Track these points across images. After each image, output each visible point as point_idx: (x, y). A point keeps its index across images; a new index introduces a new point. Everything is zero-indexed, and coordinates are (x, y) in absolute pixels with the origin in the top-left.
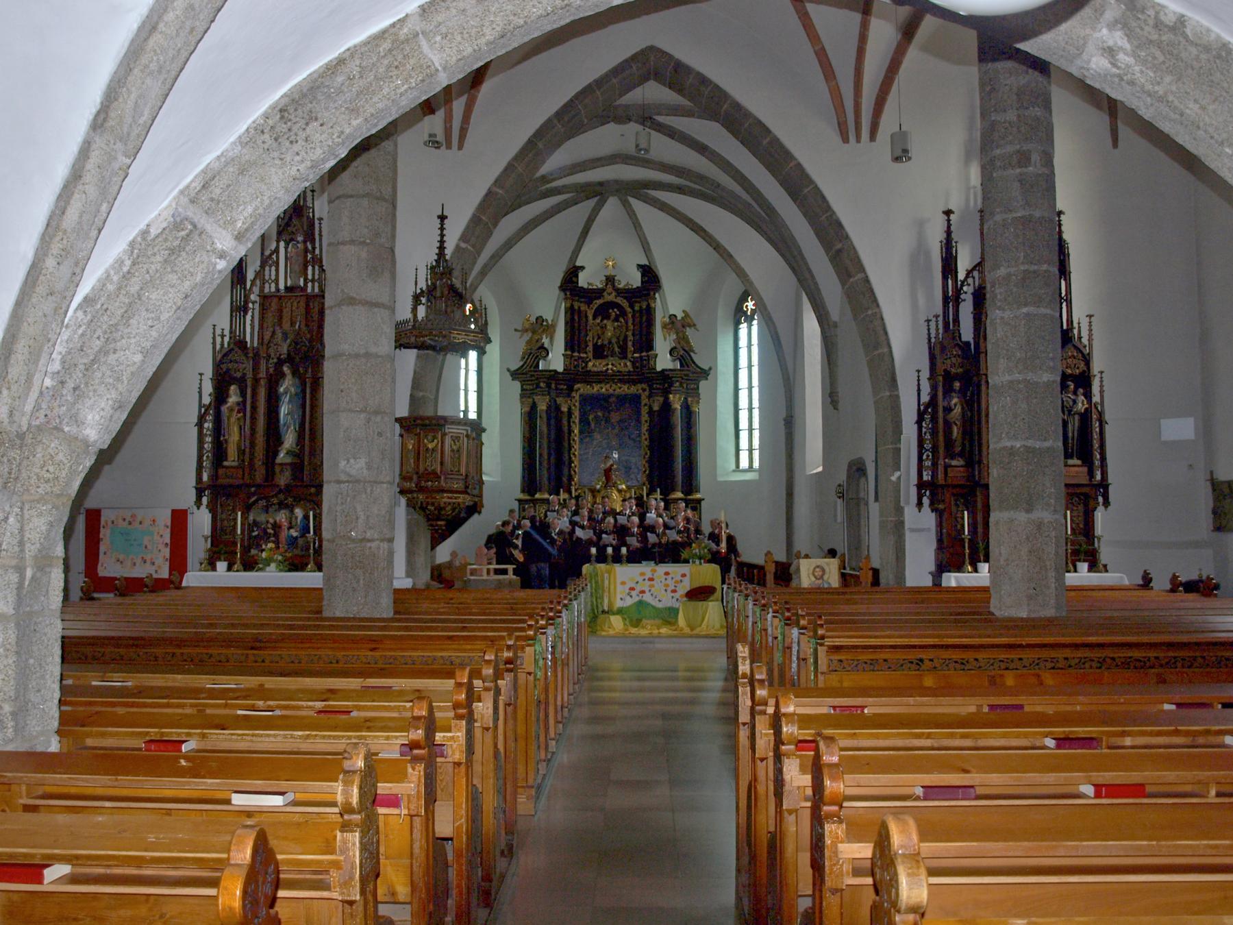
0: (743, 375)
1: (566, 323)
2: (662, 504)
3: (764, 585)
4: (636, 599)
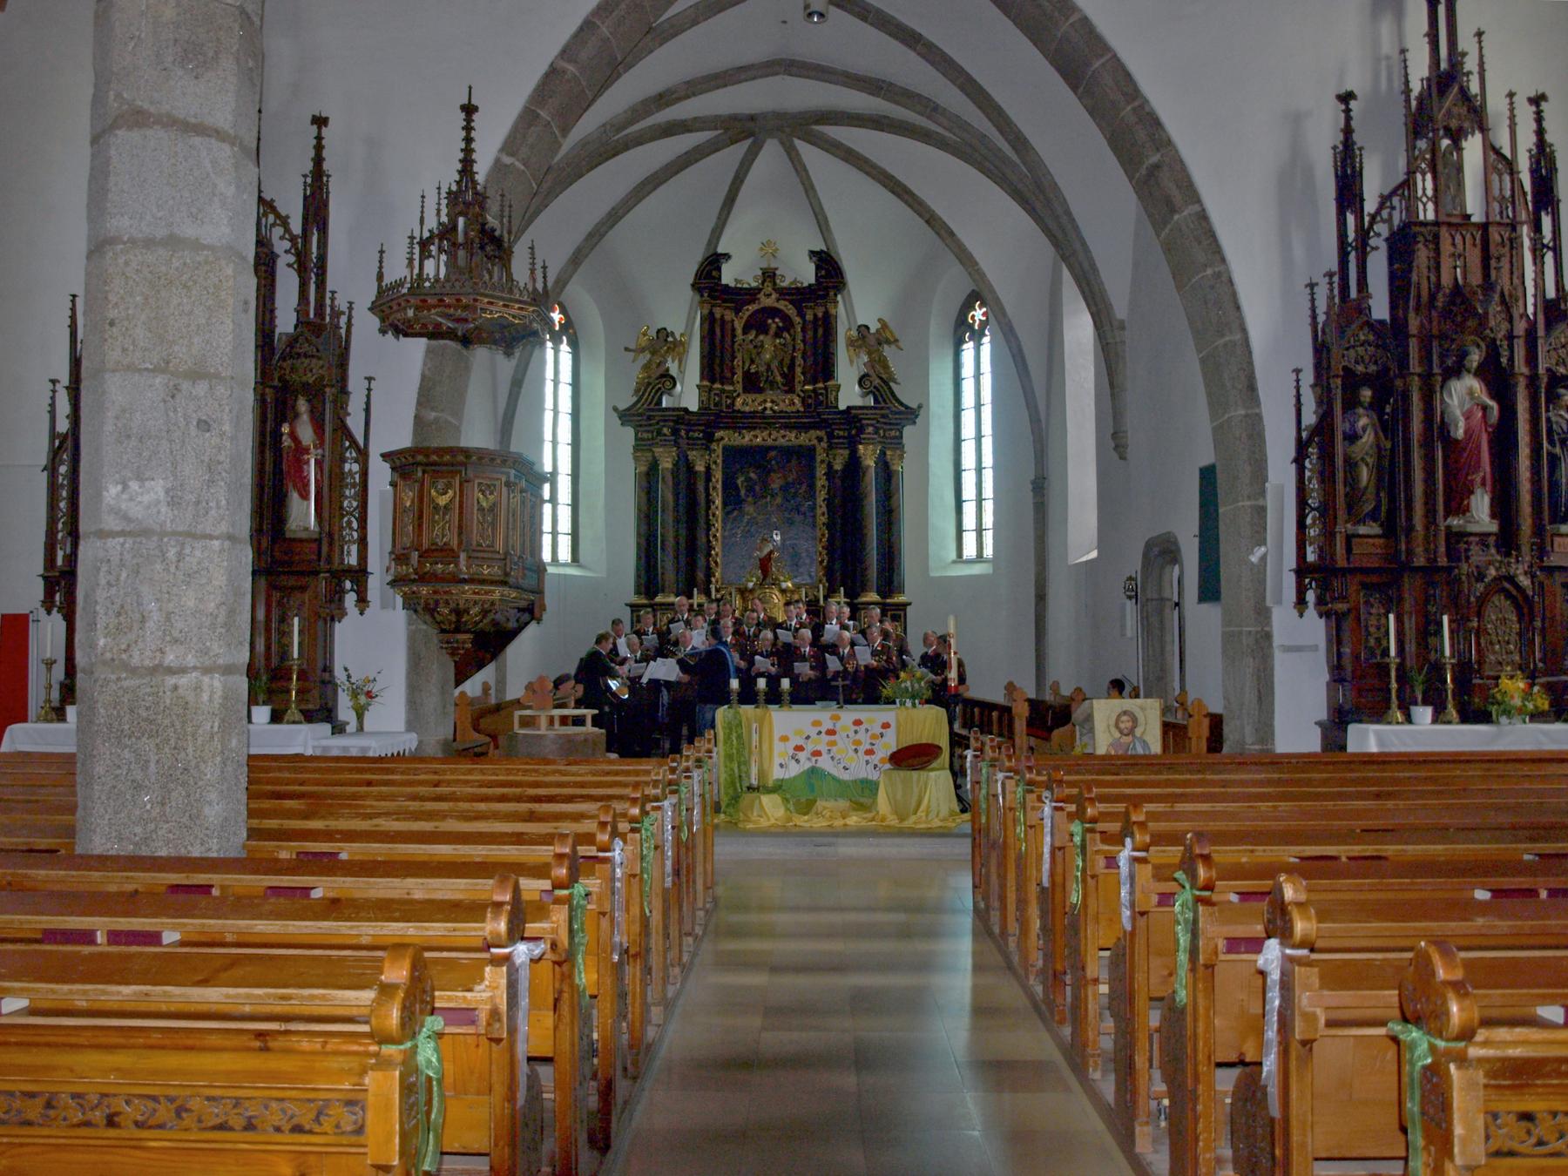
0: (968, 418)
1: (702, 339)
2: (847, 610)
3: (1011, 737)
4: (808, 765)
